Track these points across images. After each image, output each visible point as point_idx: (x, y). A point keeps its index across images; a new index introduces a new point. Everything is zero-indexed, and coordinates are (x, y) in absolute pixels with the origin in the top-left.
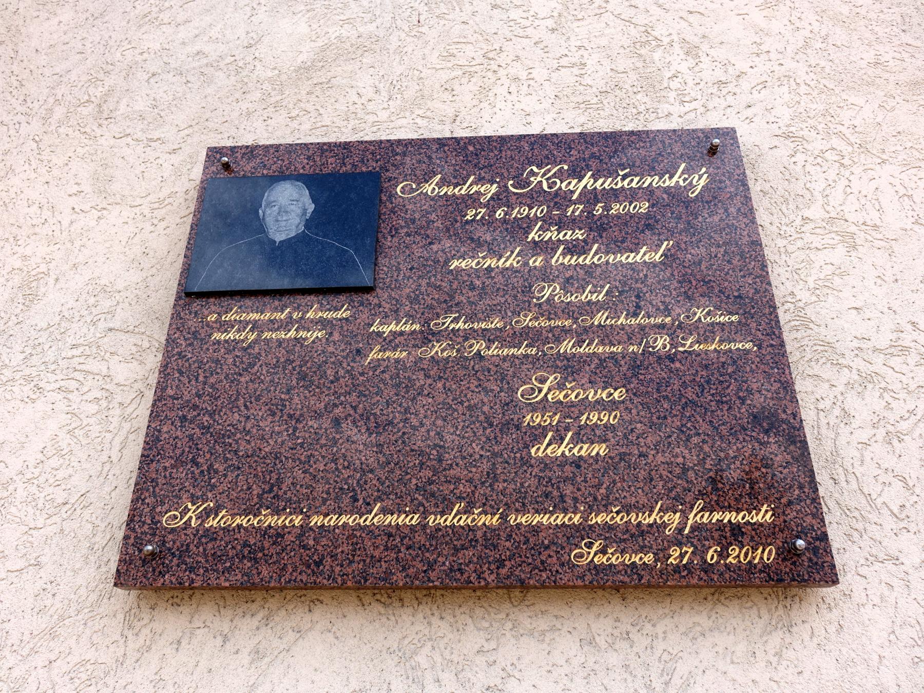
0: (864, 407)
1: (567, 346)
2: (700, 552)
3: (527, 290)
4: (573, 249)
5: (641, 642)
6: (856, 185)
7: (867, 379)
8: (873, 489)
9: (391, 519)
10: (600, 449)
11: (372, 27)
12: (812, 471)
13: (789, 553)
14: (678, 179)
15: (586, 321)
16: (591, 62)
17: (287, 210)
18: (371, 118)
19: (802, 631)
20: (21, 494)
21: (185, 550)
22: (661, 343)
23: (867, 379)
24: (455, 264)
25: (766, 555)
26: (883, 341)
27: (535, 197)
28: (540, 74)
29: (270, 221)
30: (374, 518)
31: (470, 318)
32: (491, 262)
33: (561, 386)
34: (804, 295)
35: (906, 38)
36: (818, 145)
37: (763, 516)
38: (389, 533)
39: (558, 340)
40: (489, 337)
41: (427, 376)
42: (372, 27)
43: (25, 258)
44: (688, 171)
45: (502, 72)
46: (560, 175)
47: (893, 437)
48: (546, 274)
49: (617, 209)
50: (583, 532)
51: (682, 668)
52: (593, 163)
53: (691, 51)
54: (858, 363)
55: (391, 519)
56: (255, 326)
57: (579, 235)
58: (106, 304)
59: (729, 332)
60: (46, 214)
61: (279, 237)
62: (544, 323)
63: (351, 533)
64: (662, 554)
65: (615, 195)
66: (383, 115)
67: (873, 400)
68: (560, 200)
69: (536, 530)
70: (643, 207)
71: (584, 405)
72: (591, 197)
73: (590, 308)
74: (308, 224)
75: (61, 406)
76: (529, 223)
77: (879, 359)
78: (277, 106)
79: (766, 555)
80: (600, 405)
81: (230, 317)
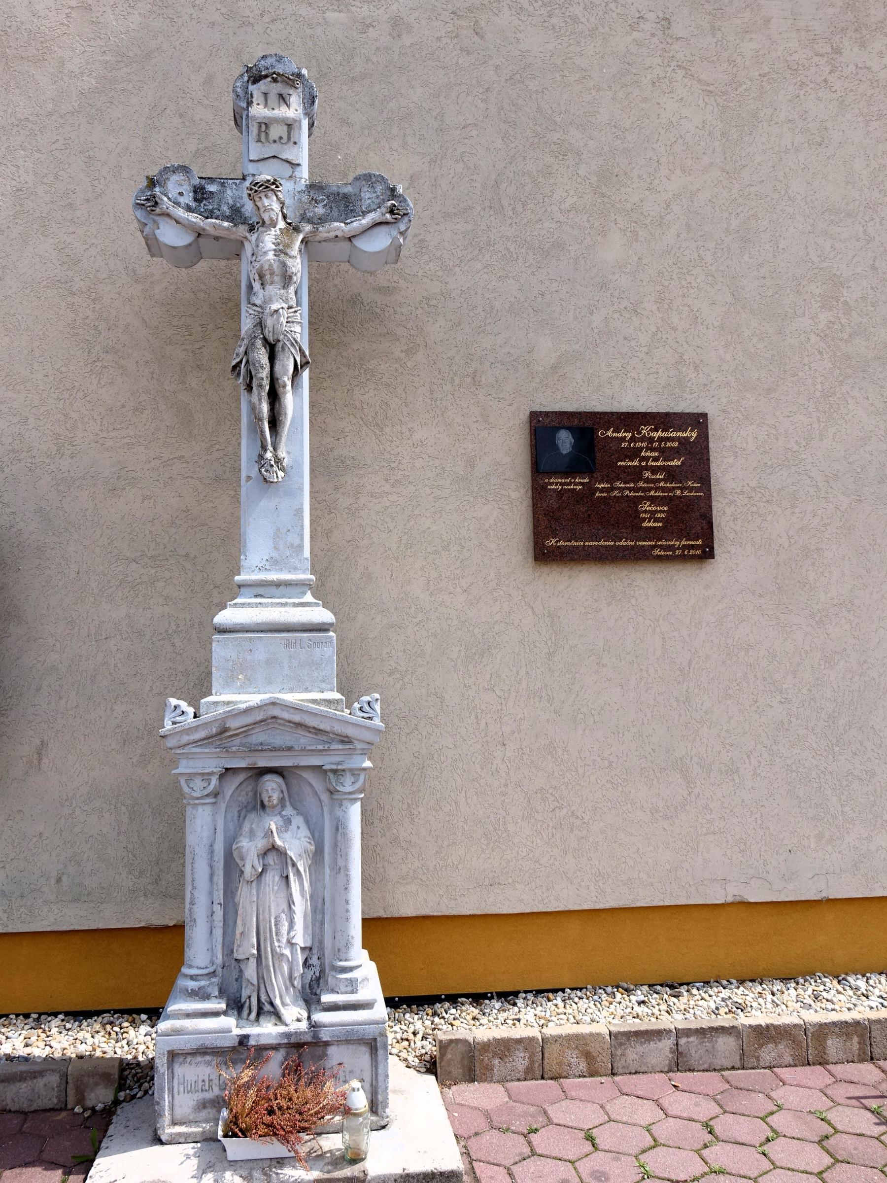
0: (729, 511)
1: (652, 493)
2: (683, 552)
3: (641, 473)
4: (656, 459)
5: (666, 572)
6: (741, 433)
7: (732, 502)
8: (727, 534)
9: (607, 543)
10: (660, 524)
11: (577, 346)
12: (712, 523)
13: (704, 552)
14: (688, 434)
15: (658, 485)
16: (661, 371)
17: (565, 441)
18: (582, 395)
19: (704, 569)
20: (492, 534)
21: (553, 552)
22: (678, 492)
23: (732, 502)
24: (619, 464)
25: (699, 552)
26: (738, 490)
27: (642, 440)
28: (642, 377)
29: (560, 445)
30: (602, 543)
31: (625, 483)
32: (630, 464)
33: (650, 506)
34: (719, 474)
35: (771, 367)
36: (732, 416)
37: (700, 542)
38: (606, 546)
39: (650, 491)
40: (630, 489)
41: (853, 677)
42: (577, 346)
43: (465, 449)
44: (692, 431)
45: (629, 375)
46: (651, 430)
47: (735, 519)
48: (647, 468)
49: (669, 444)
50: (655, 546)
51: (675, 578)
52: (662, 426)
53: (696, 368)
54: (730, 497)
55: (607, 543)
56: (561, 484)
57: (657, 454)
58: (501, 469)
59: (697, 490)
60: (467, 430)
61: (564, 452)
62: (646, 485)
63: (597, 547)
64: (674, 552)
65: (668, 439)
66: (587, 393)
67: (732, 508)
68: (651, 440)
69: (643, 546)
70: (676, 444)
71: (657, 512)
72: (661, 439)
73: (659, 480)
74: (573, 447)
75: (496, 506)
76: (641, 449)
77: (736, 496)
78: (546, 385)
79: (699, 552)
80: (661, 512)
81: (551, 481)
